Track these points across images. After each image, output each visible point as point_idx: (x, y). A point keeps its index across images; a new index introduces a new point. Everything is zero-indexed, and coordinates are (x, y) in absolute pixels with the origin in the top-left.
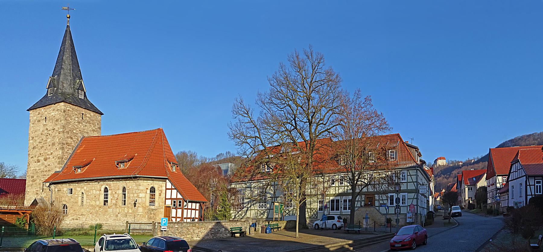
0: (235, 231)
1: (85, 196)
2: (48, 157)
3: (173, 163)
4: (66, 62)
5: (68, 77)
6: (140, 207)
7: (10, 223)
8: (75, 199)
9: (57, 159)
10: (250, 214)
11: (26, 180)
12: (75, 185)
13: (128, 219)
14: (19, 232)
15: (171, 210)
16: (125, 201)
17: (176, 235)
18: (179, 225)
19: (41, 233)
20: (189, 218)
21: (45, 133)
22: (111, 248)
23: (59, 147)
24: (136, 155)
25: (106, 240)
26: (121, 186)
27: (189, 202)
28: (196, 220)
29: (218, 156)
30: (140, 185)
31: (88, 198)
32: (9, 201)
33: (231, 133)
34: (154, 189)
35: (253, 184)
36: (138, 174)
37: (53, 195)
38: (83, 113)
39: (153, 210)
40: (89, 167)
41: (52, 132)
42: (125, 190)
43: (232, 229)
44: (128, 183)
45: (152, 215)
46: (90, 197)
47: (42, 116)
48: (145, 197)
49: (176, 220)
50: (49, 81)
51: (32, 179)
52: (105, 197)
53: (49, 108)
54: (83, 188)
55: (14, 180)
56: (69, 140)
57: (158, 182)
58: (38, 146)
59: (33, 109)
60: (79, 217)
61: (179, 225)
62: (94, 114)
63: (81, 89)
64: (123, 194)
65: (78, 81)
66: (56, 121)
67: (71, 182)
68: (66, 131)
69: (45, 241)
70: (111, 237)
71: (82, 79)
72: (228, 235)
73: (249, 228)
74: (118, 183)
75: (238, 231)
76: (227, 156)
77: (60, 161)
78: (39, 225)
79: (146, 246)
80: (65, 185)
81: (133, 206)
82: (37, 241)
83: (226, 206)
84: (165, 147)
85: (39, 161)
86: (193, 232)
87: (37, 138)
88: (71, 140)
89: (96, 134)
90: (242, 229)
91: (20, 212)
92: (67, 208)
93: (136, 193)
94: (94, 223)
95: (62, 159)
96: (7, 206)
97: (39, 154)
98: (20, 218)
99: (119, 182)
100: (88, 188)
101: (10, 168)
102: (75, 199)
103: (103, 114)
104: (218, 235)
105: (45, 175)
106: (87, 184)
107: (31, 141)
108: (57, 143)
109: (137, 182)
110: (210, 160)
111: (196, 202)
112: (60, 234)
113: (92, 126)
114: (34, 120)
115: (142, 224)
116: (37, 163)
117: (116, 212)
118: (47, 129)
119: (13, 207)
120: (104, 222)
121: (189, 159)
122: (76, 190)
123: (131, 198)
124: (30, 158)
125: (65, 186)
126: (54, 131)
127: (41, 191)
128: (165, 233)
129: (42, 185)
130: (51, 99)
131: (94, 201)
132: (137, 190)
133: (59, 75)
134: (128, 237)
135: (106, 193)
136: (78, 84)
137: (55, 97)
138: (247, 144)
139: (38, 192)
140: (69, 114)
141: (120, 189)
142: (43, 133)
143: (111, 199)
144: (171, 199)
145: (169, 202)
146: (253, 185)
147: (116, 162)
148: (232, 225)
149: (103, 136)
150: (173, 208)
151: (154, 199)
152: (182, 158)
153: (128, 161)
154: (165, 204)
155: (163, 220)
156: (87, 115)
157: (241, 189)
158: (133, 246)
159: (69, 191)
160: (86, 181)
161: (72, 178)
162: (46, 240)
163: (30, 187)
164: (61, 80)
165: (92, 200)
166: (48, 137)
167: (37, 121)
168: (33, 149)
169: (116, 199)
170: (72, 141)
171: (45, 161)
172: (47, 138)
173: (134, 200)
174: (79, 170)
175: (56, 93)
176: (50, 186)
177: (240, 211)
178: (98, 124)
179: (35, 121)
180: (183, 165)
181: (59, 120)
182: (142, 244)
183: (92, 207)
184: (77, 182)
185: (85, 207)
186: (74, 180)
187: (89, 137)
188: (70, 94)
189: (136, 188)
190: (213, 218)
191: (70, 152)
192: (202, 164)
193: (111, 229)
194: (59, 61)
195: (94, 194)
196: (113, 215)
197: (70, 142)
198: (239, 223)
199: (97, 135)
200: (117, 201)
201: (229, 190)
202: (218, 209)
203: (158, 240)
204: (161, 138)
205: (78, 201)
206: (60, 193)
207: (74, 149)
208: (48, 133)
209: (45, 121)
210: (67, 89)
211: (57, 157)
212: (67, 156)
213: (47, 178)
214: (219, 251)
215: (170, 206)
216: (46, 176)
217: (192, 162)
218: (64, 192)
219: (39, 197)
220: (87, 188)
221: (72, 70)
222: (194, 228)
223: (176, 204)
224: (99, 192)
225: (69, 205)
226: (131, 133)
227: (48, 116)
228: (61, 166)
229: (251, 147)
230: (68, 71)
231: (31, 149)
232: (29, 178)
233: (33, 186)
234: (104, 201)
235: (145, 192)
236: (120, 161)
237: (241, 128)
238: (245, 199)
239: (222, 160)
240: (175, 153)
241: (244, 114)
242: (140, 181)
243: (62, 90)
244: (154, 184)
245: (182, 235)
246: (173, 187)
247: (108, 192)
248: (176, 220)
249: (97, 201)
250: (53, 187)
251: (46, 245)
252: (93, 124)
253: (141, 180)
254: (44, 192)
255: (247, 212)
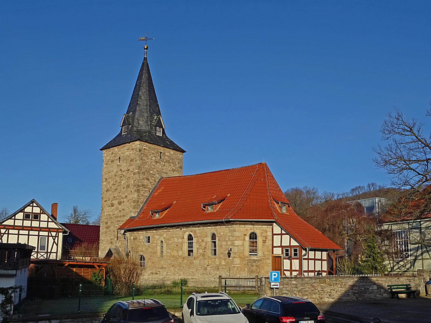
0: (398, 290)
1: (165, 245)
2: (122, 200)
3: (282, 202)
4: (143, 98)
5: (144, 114)
6: (236, 257)
7: (86, 279)
8: (153, 249)
9: (132, 203)
10: (422, 266)
11: (99, 226)
12: (153, 232)
13: (220, 272)
14: (90, 290)
15: (282, 262)
16: (215, 250)
17: (295, 294)
18: (298, 281)
19: (118, 292)
20: (312, 271)
21: (119, 175)
22: (204, 312)
23: (134, 189)
24: (229, 195)
25: (197, 301)
26: (210, 232)
27: (311, 250)
28: (324, 274)
29: (353, 190)
30: (235, 231)
31: (168, 247)
32: (84, 251)
33: (380, 159)
34: (256, 235)
35: (423, 223)
36: (231, 218)
37: (128, 244)
38: (162, 151)
39: (255, 261)
40: (168, 211)
41: (126, 173)
42: (215, 237)
43: (391, 287)
44: (218, 229)
45: (254, 268)
46: (171, 247)
47: (116, 156)
48: (243, 245)
49: (291, 274)
50: (123, 119)
51: (106, 225)
52: (189, 246)
53: (123, 147)
54: (162, 235)
55: (87, 226)
56: (145, 181)
57: (261, 226)
58: (112, 188)
59: (106, 149)
60: (159, 270)
61: (298, 281)
62: (174, 152)
63: (160, 125)
64: (212, 242)
65: (156, 117)
66: (130, 161)
67: (148, 229)
68: (142, 172)
69: (124, 302)
70: (202, 297)
71: (160, 114)
72: (385, 295)
73: (426, 286)
74: (205, 229)
75: (403, 290)
76: (370, 189)
77: (135, 206)
78: (115, 281)
79: (251, 309)
80: (142, 232)
81: (227, 256)
82: (115, 304)
83: (375, 254)
84: (270, 184)
85: (112, 205)
86: (322, 290)
87: (110, 180)
88: (147, 182)
89: (176, 174)
90: (411, 288)
91: (95, 265)
92: (144, 260)
93: (230, 241)
94: (178, 278)
95: (138, 202)
96: (81, 258)
97: (113, 197)
98: (96, 273)
99: (206, 228)
100: (168, 235)
101: (83, 212)
102: (153, 249)
103: (186, 152)
104: (366, 295)
105: (120, 221)
106: (167, 230)
107: (104, 183)
108: (132, 185)
109: (231, 227)
110: (340, 196)
111: (322, 251)
112: (139, 292)
113: (172, 165)
114: (107, 161)
115: (241, 279)
116: (110, 207)
117: (204, 264)
118: (121, 170)
119: (88, 259)
120: (190, 277)
121: (305, 196)
122: (154, 238)
123: (224, 247)
124: (103, 201)
125: (142, 233)
126: (128, 172)
127: (116, 239)
128: (277, 292)
129: (117, 232)
130: (125, 137)
131: (176, 250)
132: (232, 237)
133: (134, 112)
134: (225, 297)
135: (190, 241)
136: (155, 121)
137: (129, 136)
138: (409, 171)
139: (112, 241)
140: (145, 153)
141: (208, 236)
142: (117, 174)
143: (198, 249)
144: (281, 246)
145: (278, 251)
146: (424, 224)
147: (202, 205)
148: (390, 281)
149: (185, 176)
150: (284, 259)
151: (256, 247)
152: (294, 196)
153: (218, 203)
154: (273, 253)
155: (273, 273)
156: (166, 154)
157: (401, 231)
158: (234, 309)
159: (146, 239)
160: (166, 228)
161: (149, 224)
162: (126, 302)
163: (104, 235)
164: (136, 117)
165: (174, 250)
166: (122, 179)
167: (111, 162)
168: (106, 192)
169: (203, 248)
170: (148, 183)
171: (120, 205)
172: (121, 179)
173: (227, 249)
174: (157, 215)
175: (131, 130)
176: (125, 234)
177: (401, 261)
178: (179, 163)
179: (108, 161)
180: (295, 205)
181: (134, 160)
182: (246, 306)
183: (174, 259)
184: (155, 229)
185: (165, 258)
186: (151, 226)
187: (168, 178)
188: (146, 132)
189: (230, 234)
190: (354, 271)
191: (147, 194)
192: (326, 201)
193: (200, 286)
194: (134, 97)
195: (176, 243)
196: (200, 268)
197: (147, 184)
198: (404, 278)
199: (178, 175)
200: (205, 250)
201: (380, 233)
202: (359, 259)
203: (268, 302)
204: (264, 174)
205: (157, 251)
206: (136, 242)
207: (151, 191)
208: (122, 175)
209: (119, 161)
210: (143, 126)
211: (133, 201)
212: (143, 199)
213: (121, 225)
214: (374, 319)
215: (280, 256)
216: (121, 222)
217: (310, 200)
218: (141, 241)
219: (113, 247)
220: (166, 236)
221: (150, 105)
222: (322, 285)
223: (289, 252)
224: (181, 240)
225: (146, 255)
226: (222, 171)
227: (122, 156)
228: (136, 210)
229: (419, 174)
230: (144, 106)
231: (104, 191)
232: (103, 224)
233: (107, 233)
234: (189, 250)
235: (242, 238)
236: (207, 203)
237: (398, 151)
238: (409, 245)
239: (362, 194)
240: (284, 190)
241: (404, 131)
242: (234, 226)
243: (138, 127)
244: (255, 229)
245: (303, 295)
246: (283, 232)
247: (193, 240)
248: (291, 274)
249: (179, 250)
250: (128, 234)
251: (126, 308)
252: (173, 163)
253: (236, 224)
254: (118, 241)
255: (415, 262)
